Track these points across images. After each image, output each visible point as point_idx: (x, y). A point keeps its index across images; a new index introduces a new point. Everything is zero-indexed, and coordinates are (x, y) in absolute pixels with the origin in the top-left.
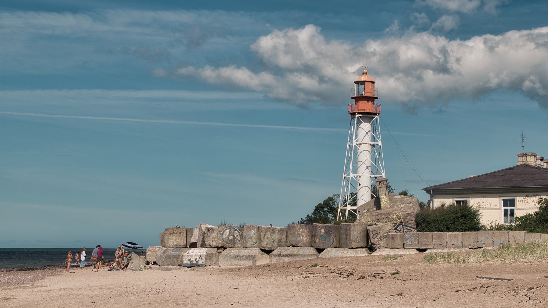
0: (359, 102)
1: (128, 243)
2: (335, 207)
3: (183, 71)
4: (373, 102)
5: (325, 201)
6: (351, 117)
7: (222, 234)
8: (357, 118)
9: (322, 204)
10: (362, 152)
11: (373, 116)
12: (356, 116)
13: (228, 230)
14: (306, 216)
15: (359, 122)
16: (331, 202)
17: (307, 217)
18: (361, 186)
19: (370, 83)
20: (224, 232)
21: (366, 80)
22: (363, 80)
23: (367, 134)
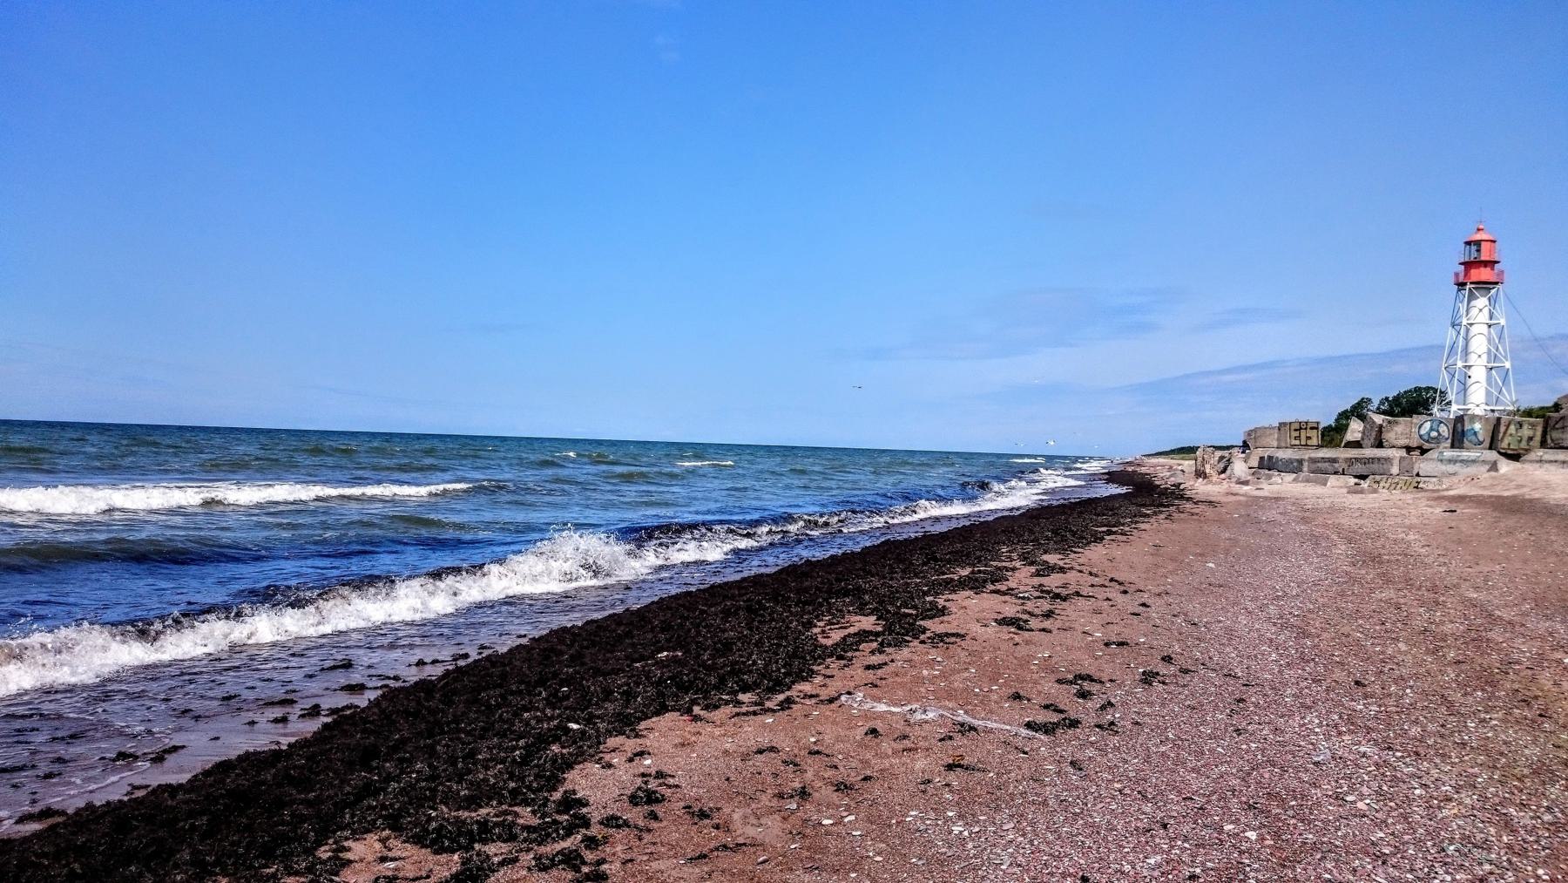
3: (1123, 490)
4: (1493, 269)
7: (1420, 427)
8: (1470, 289)
11: (1491, 286)
13: (1429, 423)
15: (1472, 297)
19: (1489, 243)
20: (1422, 424)
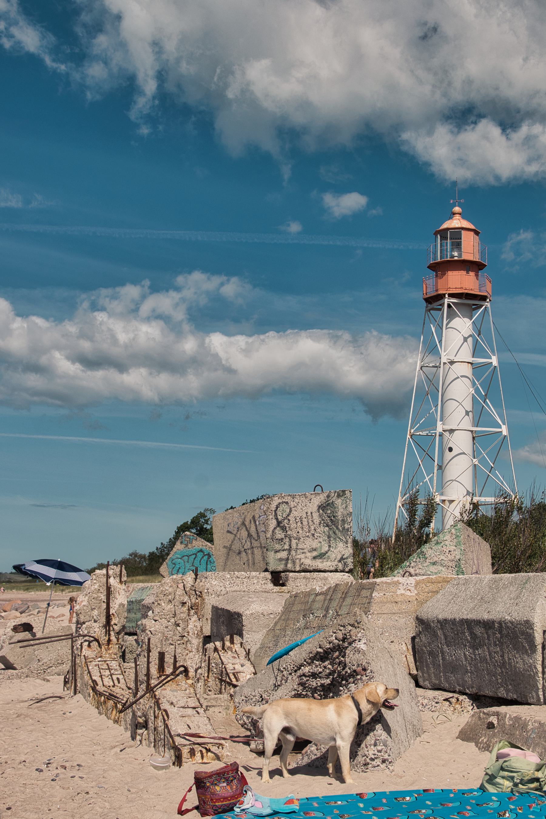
0: (449, 272)
1: (39, 562)
2: (209, 527)
5: (193, 518)
6: (426, 307)
9: (189, 523)
10: (458, 378)
12: (447, 301)
14: (168, 541)
15: (451, 316)
16: (202, 520)
17: (170, 541)
18: (454, 453)
21: (464, 226)
22: (457, 226)
23: (467, 342)
